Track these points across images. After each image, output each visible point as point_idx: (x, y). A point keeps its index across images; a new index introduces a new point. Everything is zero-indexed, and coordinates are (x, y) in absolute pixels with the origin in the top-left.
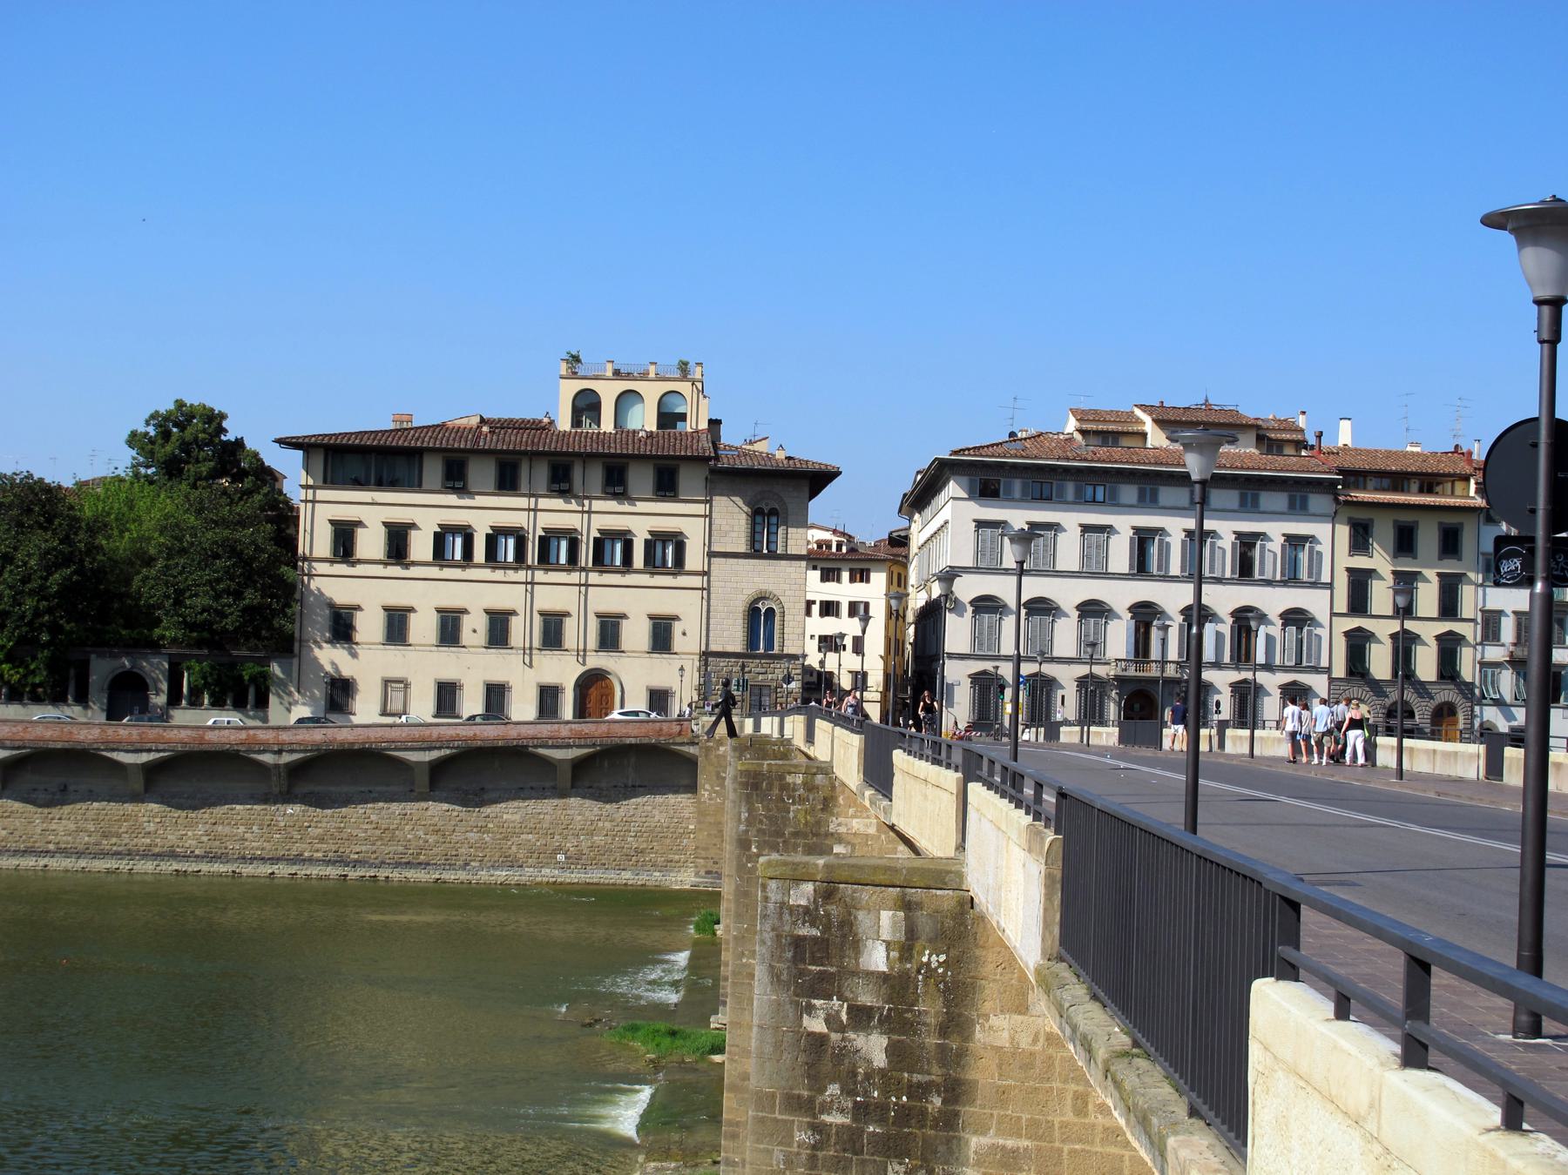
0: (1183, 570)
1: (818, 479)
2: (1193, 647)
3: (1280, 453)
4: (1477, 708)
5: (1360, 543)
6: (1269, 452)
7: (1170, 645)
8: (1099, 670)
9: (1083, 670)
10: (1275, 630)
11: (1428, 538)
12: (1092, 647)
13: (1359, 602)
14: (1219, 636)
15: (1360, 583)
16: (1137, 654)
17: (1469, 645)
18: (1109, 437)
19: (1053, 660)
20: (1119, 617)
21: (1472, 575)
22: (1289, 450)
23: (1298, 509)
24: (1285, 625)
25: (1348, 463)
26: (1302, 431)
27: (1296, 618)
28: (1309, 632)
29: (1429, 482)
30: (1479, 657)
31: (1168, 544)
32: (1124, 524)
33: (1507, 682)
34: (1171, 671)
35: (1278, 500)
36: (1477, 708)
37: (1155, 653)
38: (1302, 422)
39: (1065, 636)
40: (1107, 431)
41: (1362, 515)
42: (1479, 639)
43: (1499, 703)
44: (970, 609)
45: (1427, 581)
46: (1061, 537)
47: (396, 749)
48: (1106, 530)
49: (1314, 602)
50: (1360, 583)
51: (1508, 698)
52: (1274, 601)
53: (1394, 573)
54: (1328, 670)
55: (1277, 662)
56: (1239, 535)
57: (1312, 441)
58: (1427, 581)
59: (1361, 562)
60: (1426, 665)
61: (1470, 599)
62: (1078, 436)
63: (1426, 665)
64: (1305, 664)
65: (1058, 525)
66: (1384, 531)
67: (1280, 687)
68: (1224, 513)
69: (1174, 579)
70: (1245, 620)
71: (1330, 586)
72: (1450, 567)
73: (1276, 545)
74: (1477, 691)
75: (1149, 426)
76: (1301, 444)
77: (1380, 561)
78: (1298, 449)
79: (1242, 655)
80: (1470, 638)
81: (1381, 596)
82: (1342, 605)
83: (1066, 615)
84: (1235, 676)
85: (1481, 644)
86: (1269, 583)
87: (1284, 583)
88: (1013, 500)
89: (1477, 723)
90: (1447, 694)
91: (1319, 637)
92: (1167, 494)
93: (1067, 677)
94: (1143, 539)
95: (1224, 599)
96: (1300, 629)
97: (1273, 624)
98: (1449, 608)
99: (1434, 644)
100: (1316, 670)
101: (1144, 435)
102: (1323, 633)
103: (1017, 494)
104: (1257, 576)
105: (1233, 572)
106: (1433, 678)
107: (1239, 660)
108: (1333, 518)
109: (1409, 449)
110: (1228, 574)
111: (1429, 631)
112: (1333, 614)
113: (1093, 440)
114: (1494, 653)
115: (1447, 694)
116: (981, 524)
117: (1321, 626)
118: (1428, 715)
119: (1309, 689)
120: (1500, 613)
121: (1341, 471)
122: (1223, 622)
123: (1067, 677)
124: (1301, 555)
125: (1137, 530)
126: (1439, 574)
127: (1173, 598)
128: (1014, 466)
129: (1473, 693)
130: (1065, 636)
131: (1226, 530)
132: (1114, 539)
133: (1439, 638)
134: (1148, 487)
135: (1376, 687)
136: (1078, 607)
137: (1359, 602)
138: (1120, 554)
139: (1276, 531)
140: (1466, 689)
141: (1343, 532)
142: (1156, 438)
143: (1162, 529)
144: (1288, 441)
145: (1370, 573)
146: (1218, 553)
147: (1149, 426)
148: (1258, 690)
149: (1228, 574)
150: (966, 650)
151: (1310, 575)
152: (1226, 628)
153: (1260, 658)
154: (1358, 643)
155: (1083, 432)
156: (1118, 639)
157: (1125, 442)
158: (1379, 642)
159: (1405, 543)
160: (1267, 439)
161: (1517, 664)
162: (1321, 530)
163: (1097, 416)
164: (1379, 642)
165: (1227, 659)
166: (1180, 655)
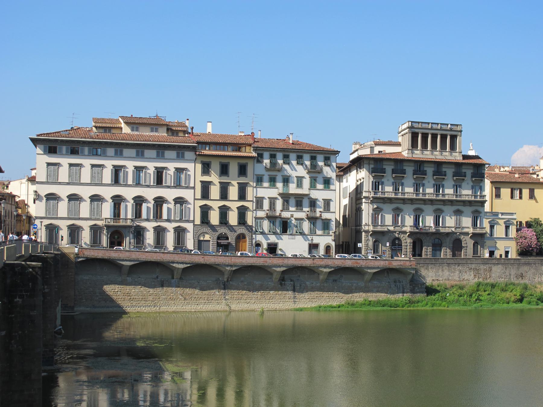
0: (133, 182)
1: (338, 152)
2: (138, 214)
3: (177, 135)
4: (254, 236)
5: (206, 169)
6: (173, 135)
7: (128, 211)
8: (100, 223)
9: (92, 223)
10: (172, 206)
11: (234, 169)
12: (74, 214)
13: (205, 195)
14: (148, 208)
15: (206, 187)
16: (114, 216)
17: (250, 211)
18: (107, 129)
19: (57, 218)
20: (107, 201)
21: (251, 183)
22: (181, 134)
23: (180, 157)
24: (175, 204)
25: (202, 139)
26: (186, 126)
27: (179, 201)
28: (185, 206)
29: (238, 147)
30: (254, 215)
31: (127, 172)
32: (109, 164)
33: (266, 225)
34: (129, 223)
35: (172, 154)
36: (254, 236)
37: (122, 216)
38: (187, 124)
39: (85, 209)
40: (106, 127)
41: (206, 160)
42: (254, 208)
43: (263, 233)
44: (45, 199)
45: (233, 186)
46: (61, 168)
47: (123, 260)
48: (80, 165)
49: (187, 194)
50: (206, 187)
51: (266, 231)
52: (170, 194)
53: (220, 182)
54: (193, 221)
55: (172, 218)
56: (156, 168)
57: (190, 131)
58: (233, 186)
59: (206, 178)
60: (233, 218)
61: (250, 193)
62: (94, 129)
63: (233, 218)
64: (183, 219)
65: (103, 165)
66: (215, 166)
67: (173, 228)
68: (150, 159)
69: (130, 186)
70: (159, 202)
71: (194, 188)
72: (243, 180)
73: (171, 172)
74: (254, 229)
75: (123, 125)
76: (185, 132)
77: (214, 178)
78: (184, 134)
79: (158, 215)
80: (251, 208)
81: (215, 192)
82: (199, 195)
83: (85, 201)
84: (155, 224)
85: (255, 210)
86: (169, 187)
87: (175, 187)
88: (63, 154)
89: (254, 241)
90: (242, 230)
91: (190, 208)
92: (127, 152)
93: (86, 225)
94: (117, 170)
95: (151, 194)
96: (182, 205)
97: (170, 203)
98: (242, 196)
99: (236, 211)
100: (188, 221)
101: (121, 128)
102: (191, 207)
103: (86, 152)
104: (164, 184)
105: (154, 183)
106: (236, 224)
107: (157, 218)
108: (195, 161)
109: (240, 134)
110: (152, 184)
111: (234, 205)
112: (195, 199)
113: (102, 130)
114: (261, 214)
115: (242, 230)
116: (49, 164)
117: (190, 204)
118: (234, 238)
119: (186, 229)
120: (263, 198)
121: (198, 143)
122: (150, 203)
123: (86, 225)
124: (182, 176)
125: (156, 168)
126: (238, 183)
127: (129, 193)
128: (62, 141)
129: (252, 230)
130: (85, 209)
131: (151, 166)
132: (105, 170)
133: (238, 208)
134: (119, 149)
135: (213, 228)
136: (68, 197)
137: (205, 195)
138: (107, 176)
139: (171, 166)
140: (249, 229)
141: (199, 166)
142: (126, 130)
143: (125, 166)
144: (180, 131)
145: (210, 183)
146: (148, 175)
147: (123, 125)
148: (144, 229)
149: (152, 184)
150: (88, 216)
151: (185, 184)
152: (151, 205)
153: (165, 216)
154: (205, 211)
155: (96, 127)
156: (107, 210)
157: (113, 131)
158: (232, 210)
159: (224, 170)
160: (170, 130)
161: (269, 217)
162: (189, 166)
163: (103, 120)
164: (232, 210)
165: (152, 218)
166: (132, 216)
